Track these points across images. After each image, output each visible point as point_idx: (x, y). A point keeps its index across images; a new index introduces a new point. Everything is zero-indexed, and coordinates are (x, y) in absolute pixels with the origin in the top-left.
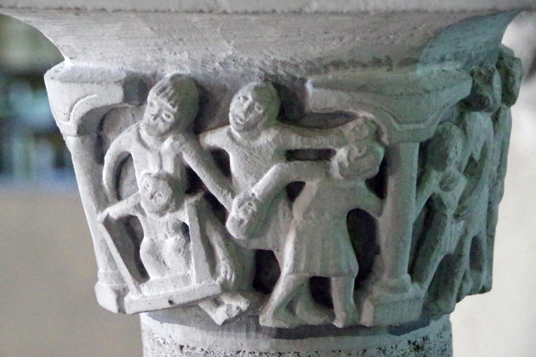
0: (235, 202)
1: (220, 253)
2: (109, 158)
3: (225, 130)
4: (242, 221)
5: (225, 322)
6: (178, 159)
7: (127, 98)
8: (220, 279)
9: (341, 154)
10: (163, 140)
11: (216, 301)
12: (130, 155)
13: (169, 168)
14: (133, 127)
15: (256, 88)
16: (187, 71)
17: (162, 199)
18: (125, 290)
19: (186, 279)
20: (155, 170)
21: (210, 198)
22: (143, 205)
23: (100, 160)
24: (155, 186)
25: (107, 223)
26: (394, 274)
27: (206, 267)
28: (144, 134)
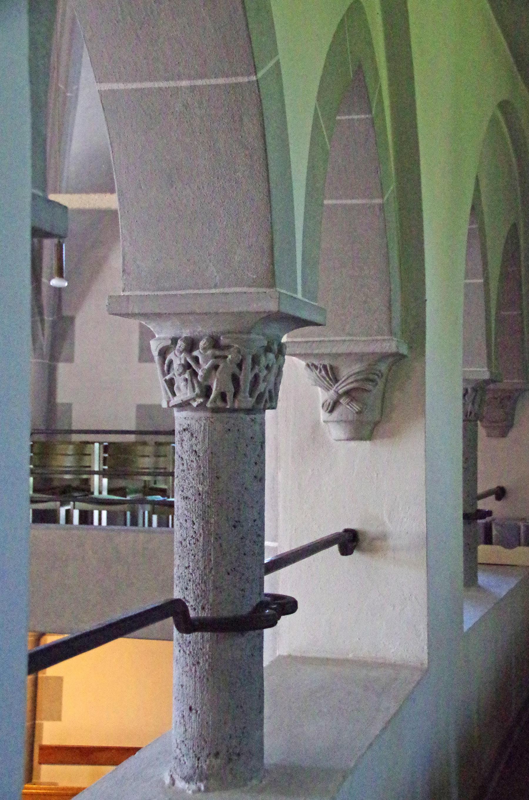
0: (200, 371)
1: (196, 385)
2: (167, 362)
3: (198, 351)
4: (202, 375)
5: (197, 406)
6: (185, 360)
7: (172, 343)
8: (196, 393)
9: (230, 357)
10: (181, 354)
11: (194, 399)
12: (172, 361)
13: (183, 362)
14: (174, 352)
15: (207, 339)
16: (189, 335)
17: (181, 371)
18: (170, 401)
19: (186, 394)
20: (179, 363)
21: (194, 370)
22: (175, 374)
23: (164, 363)
24: (179, 367)
25: (166, 381)
26: (244, 392)
27: (192, 389)
28: (176, 352)
